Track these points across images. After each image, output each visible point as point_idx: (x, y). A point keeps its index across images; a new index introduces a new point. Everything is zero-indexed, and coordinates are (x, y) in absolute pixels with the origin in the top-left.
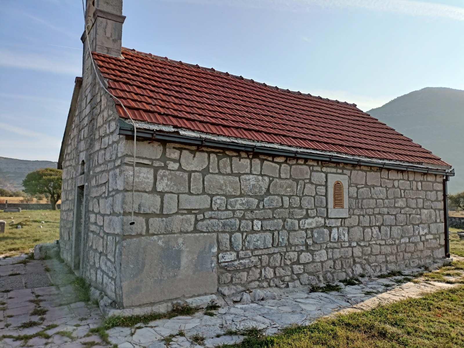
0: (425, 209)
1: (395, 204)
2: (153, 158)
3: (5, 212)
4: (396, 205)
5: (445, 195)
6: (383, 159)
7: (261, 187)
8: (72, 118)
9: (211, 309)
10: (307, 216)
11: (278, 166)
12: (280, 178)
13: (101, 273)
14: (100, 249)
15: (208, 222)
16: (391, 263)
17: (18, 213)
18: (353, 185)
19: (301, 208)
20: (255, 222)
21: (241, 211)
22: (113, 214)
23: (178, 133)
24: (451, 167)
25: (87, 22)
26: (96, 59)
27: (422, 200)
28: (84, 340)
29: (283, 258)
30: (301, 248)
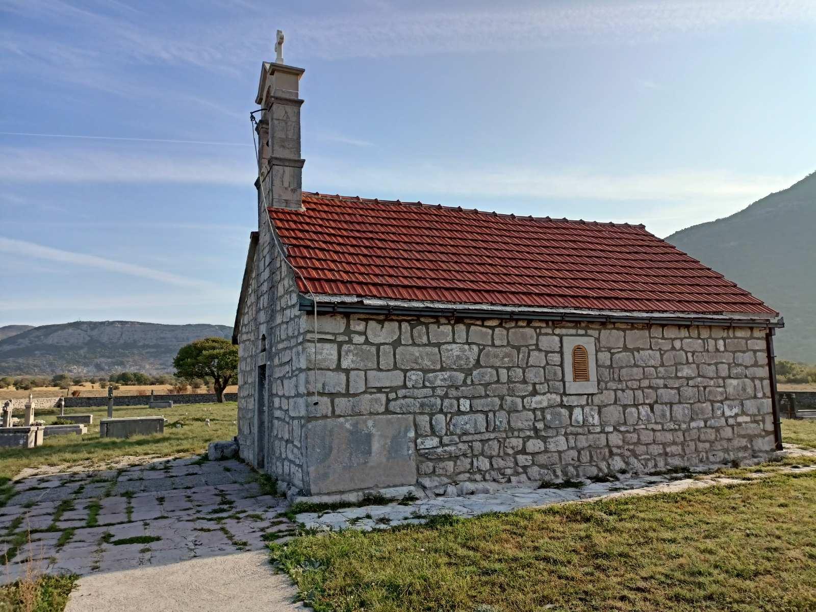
0: (732, 378)
1: (676, 373)
2: (337, 332)
3: (150, 408)
4: (679, 374)
5: (770, 358)
6: (652, 312)
7: (468, 358)
8: (248, 281)
9: (408, 499)
10: (534, 393)
11: (490, 331)
12: (493, 345)
13: (288, 463)
14: (286, 436)
15: (402, 401)
16: (673, 455)
17: (168, 409)
18: (603, 349)
19: (524, 382)
20: (462, 401)
21: (442, 388)
22: (298, 395)
23: (362, 302)
24: (777, 314)
25: (260, 167)
26: (274, 219)
27: (726, 366)
28: (272, 520)
29: (502, 445)
30: (528, 433)
